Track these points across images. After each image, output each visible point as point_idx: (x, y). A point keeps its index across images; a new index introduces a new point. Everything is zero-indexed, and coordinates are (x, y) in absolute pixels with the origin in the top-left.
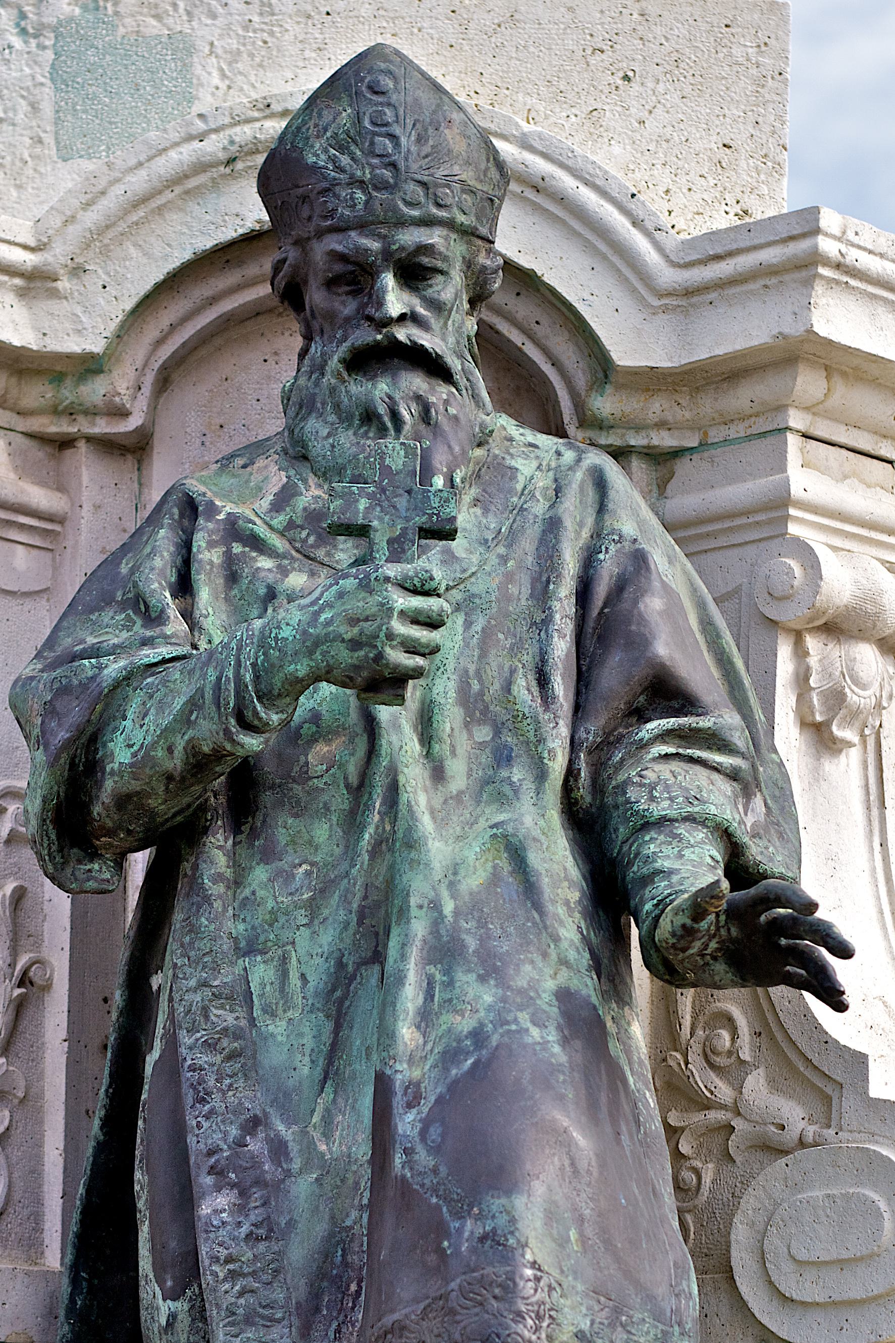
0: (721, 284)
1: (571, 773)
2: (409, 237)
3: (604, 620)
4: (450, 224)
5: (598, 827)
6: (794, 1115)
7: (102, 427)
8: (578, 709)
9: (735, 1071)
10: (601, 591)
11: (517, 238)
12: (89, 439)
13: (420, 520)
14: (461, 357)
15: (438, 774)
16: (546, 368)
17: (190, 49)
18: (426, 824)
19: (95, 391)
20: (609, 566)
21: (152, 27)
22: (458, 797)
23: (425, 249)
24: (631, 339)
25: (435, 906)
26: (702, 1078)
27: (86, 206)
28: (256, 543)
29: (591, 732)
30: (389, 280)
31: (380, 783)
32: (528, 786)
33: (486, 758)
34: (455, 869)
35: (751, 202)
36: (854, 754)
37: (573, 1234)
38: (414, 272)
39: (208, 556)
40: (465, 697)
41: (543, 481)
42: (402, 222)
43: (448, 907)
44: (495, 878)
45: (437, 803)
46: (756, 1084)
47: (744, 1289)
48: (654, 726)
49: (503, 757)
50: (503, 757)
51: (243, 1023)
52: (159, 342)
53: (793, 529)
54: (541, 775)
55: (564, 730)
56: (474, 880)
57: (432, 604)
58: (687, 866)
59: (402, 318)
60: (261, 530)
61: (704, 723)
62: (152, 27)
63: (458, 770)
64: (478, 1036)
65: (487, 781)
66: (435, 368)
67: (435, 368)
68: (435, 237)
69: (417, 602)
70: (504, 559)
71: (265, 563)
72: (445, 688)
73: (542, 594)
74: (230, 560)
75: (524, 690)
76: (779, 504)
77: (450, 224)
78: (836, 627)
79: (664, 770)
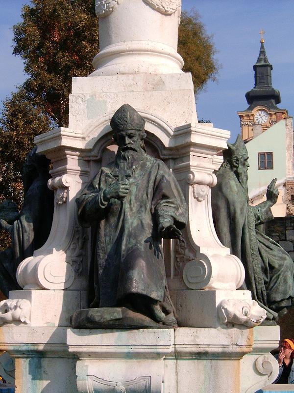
0: (180, 134)
1: (151, 209)
2: (129, 132)
3: (157, 187)
4: (135, 129)
5: (155, 217)
6: (191, 255)
7: (94, 159)
8: (152, 200)
9: (184, 249)
10: (157, 183)
11: (149, 127)
12: (92, 160)
13: (126, 174)
14: (139, 148)
15: (131, 210)
16: (157, 147)
17: (106, 103)
18: (129, 217)
19: (93, 153)
20: (159, 178)
21: (101, 99)
22: (134, 213)
23: (131, 133)
24: (166, 141)
25: (129, 229)
26: (180, 250)
27: (89, 128)
28: (110, 177)
29: (154, 203)
30: (127, 138)
31: (123, 211)
32: (144, 211)
33: (139, 207)
34: (132, 223)
35: (188, 121)
36: (203, 201)
37: (142, 275)
38: (130, 137)
39: (103, 179)
40: (136, 199)
41: (150, 165)
42: (128, 130)
43: (130, 229)
44: (138, 225)
45: (131, 213)
46: (187, 251)
47: (185, 281)
48: (162, 201)
49: (141, 207)
50: (141, 207)
51: (105, 246)
52: (102, 146)
53: (191, 169)
54: (146, 209)
55: (150, 202)
56: (135, 224)
57: (127, 187)
58: (166, 222)
59: (129, 143)
60: (110, 175)
61: (170, 200)
62: (101, 99)
63: (134, 209)
64: (132, 247)
65: (139, 210)
66: (134, 150)
67: (134, 150)
68: (133, 131)
69: (124, 186)
70: (143, 178)
71: (110, 180)
72: (133, 197)
73: (148, 182)
74: (106, 180)
75: (145, 196)
76: (188, 166)
77: (135, 129)
78: (199, 183)
79: (163, 208)
